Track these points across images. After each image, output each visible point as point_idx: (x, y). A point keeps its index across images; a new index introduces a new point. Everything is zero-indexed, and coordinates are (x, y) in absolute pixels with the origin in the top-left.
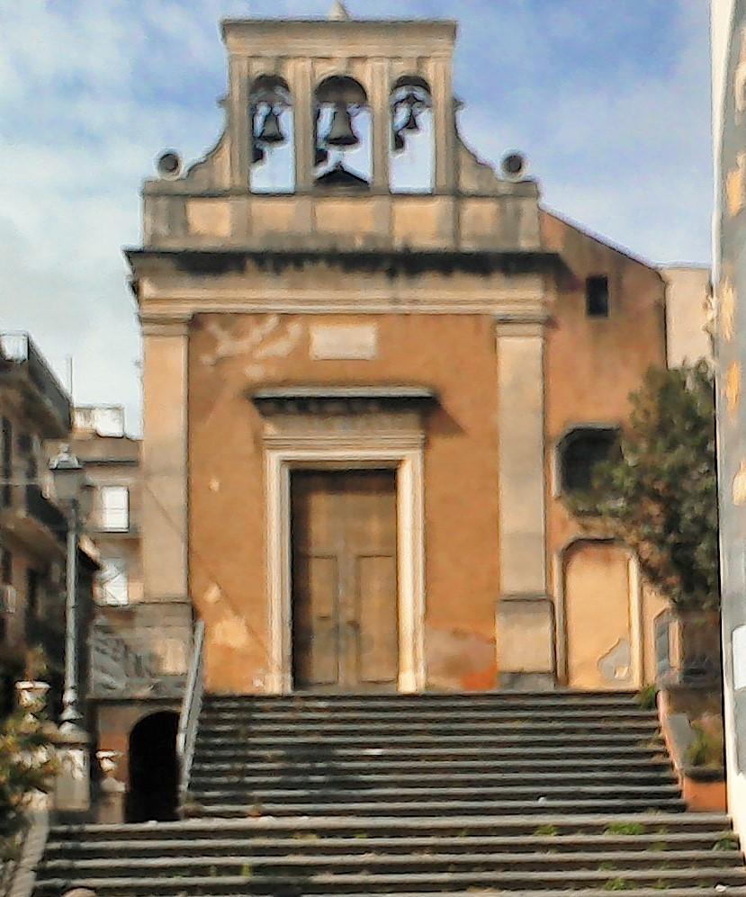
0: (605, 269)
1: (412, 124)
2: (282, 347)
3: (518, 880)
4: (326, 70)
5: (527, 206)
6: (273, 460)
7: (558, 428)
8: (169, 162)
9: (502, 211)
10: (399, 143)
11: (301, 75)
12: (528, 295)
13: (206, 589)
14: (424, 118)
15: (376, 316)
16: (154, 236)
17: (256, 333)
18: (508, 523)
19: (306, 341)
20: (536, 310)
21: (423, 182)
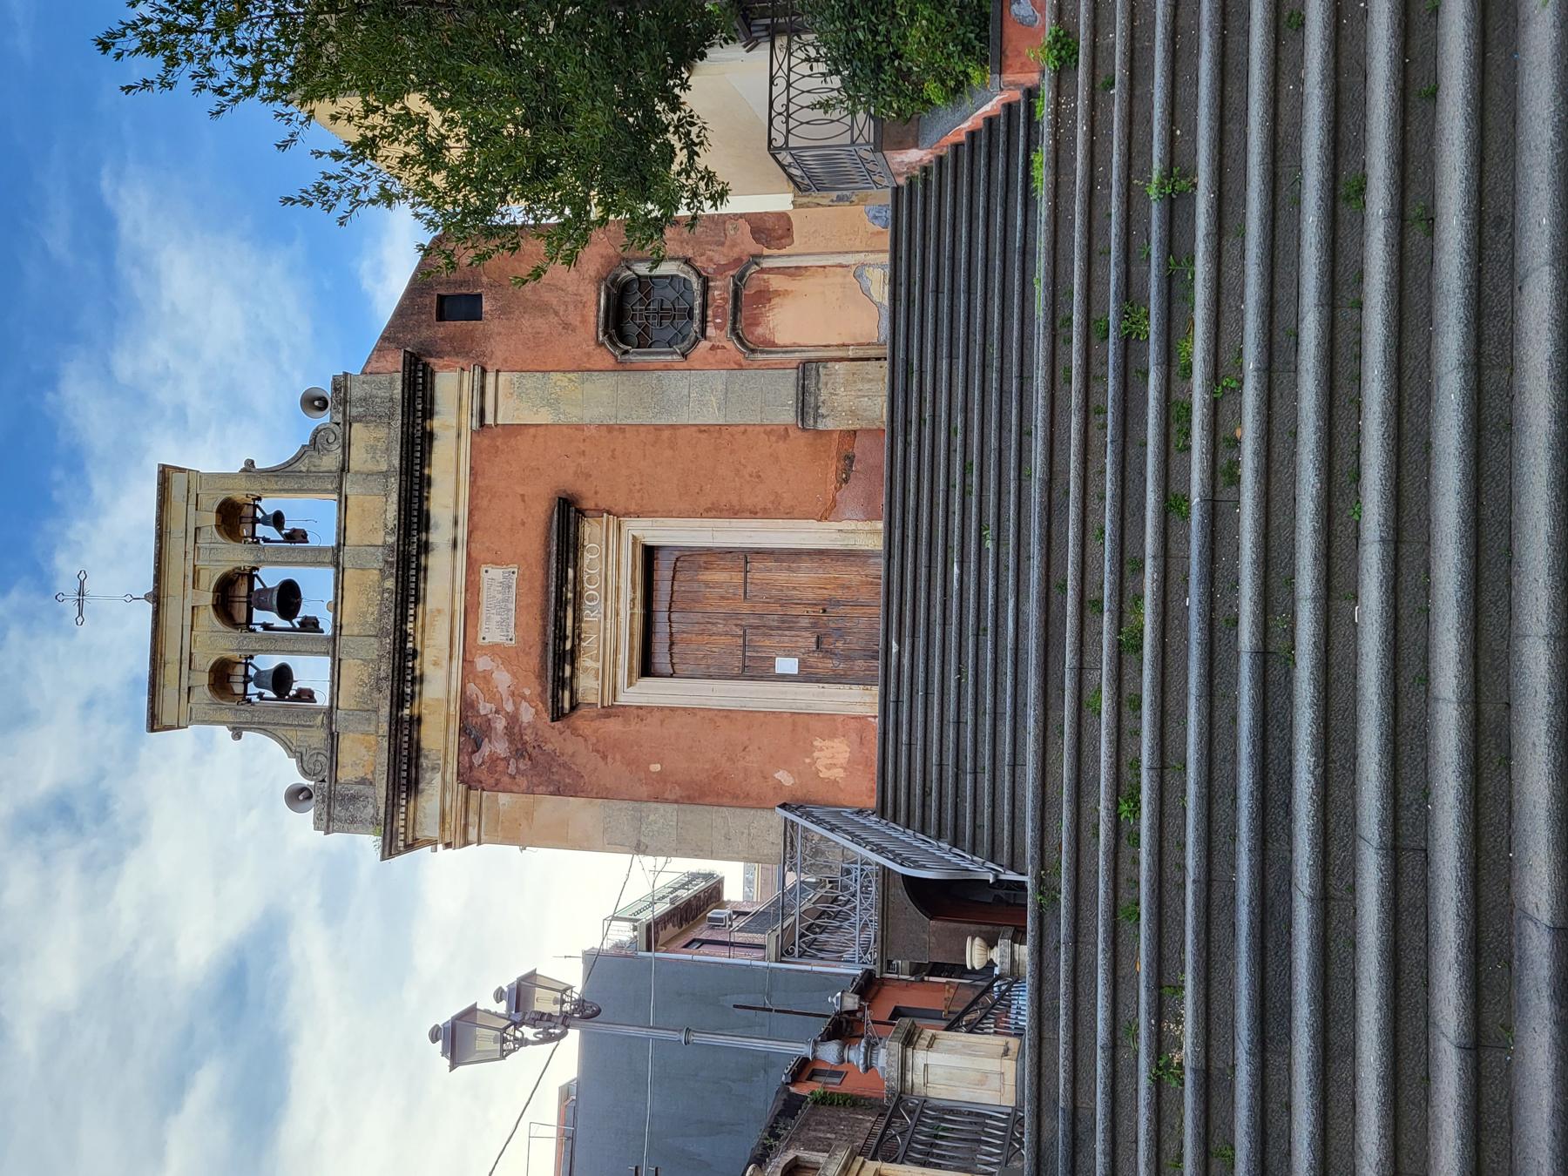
0: (431, 302)
1: (277, 520)
2: (503, 679)
3: (1433, 165)
4: (208, 617)
5: (356, 392)
6: (628, 697)
7: (604, 358)
8: (297, 797)
9: (359, 419)
10: (297, 536)
11: (214, 641)
12: (449, 385)
13: (779, 786)
14: (268, 505)
15: (472, 566)
16: (374, 821)
17: (485, 708)
18: (711, 415)
19: (494, 650)
20: (896, 1047)
21: (329, 503)
